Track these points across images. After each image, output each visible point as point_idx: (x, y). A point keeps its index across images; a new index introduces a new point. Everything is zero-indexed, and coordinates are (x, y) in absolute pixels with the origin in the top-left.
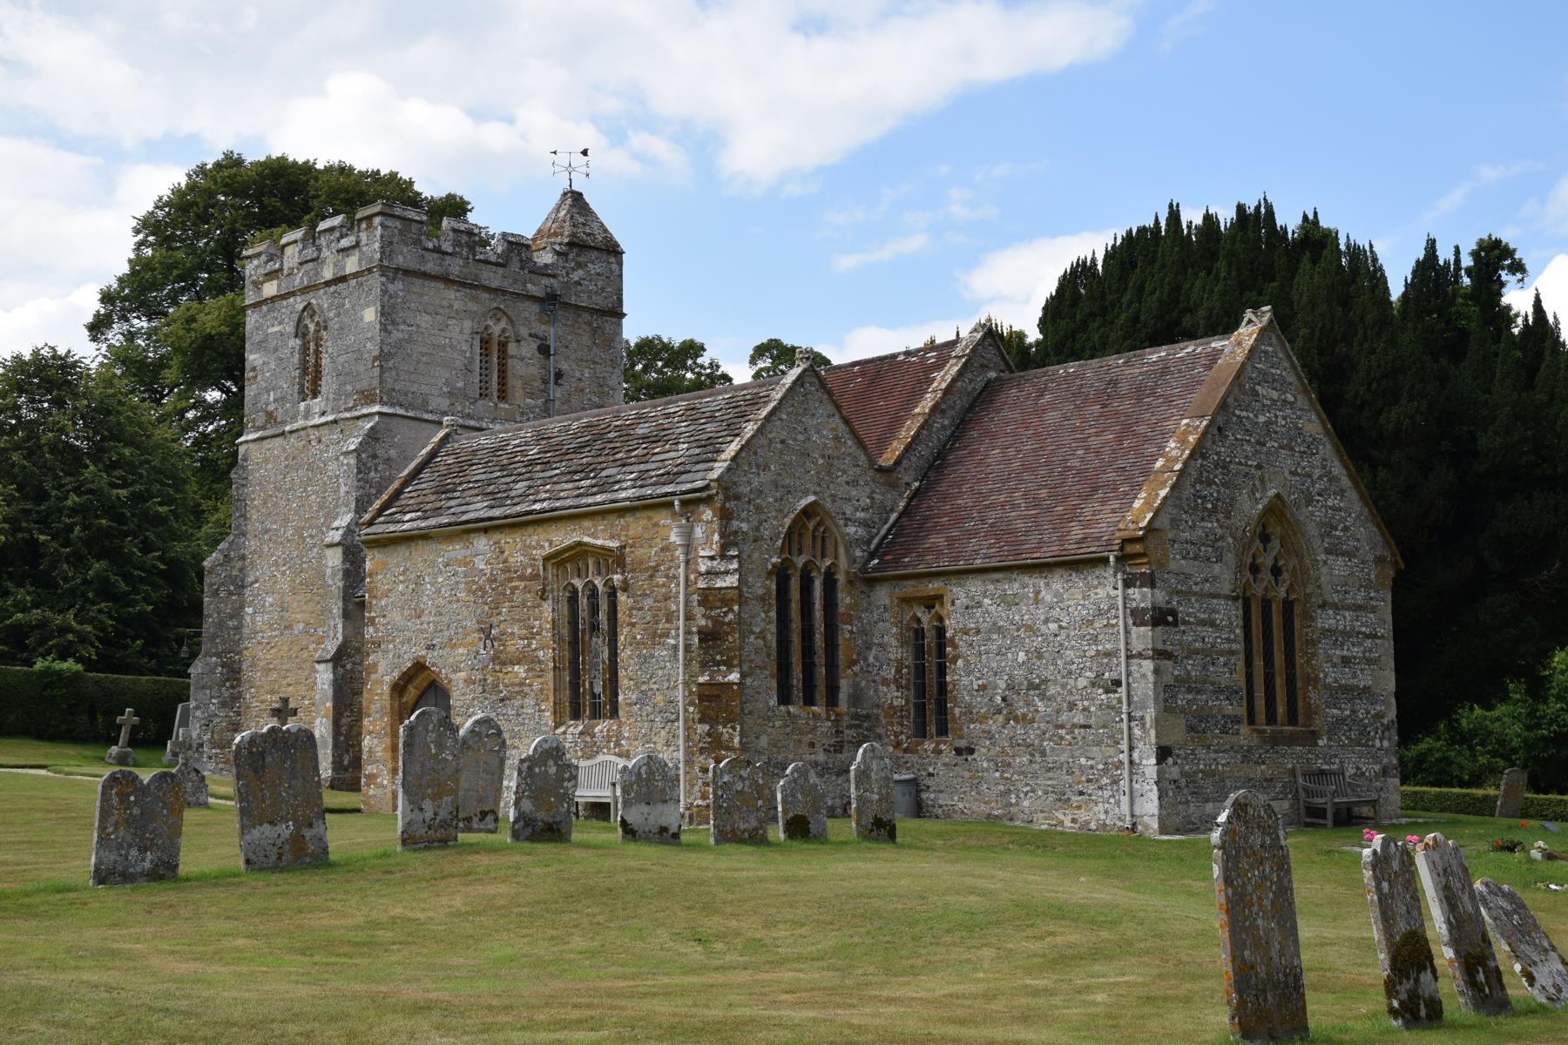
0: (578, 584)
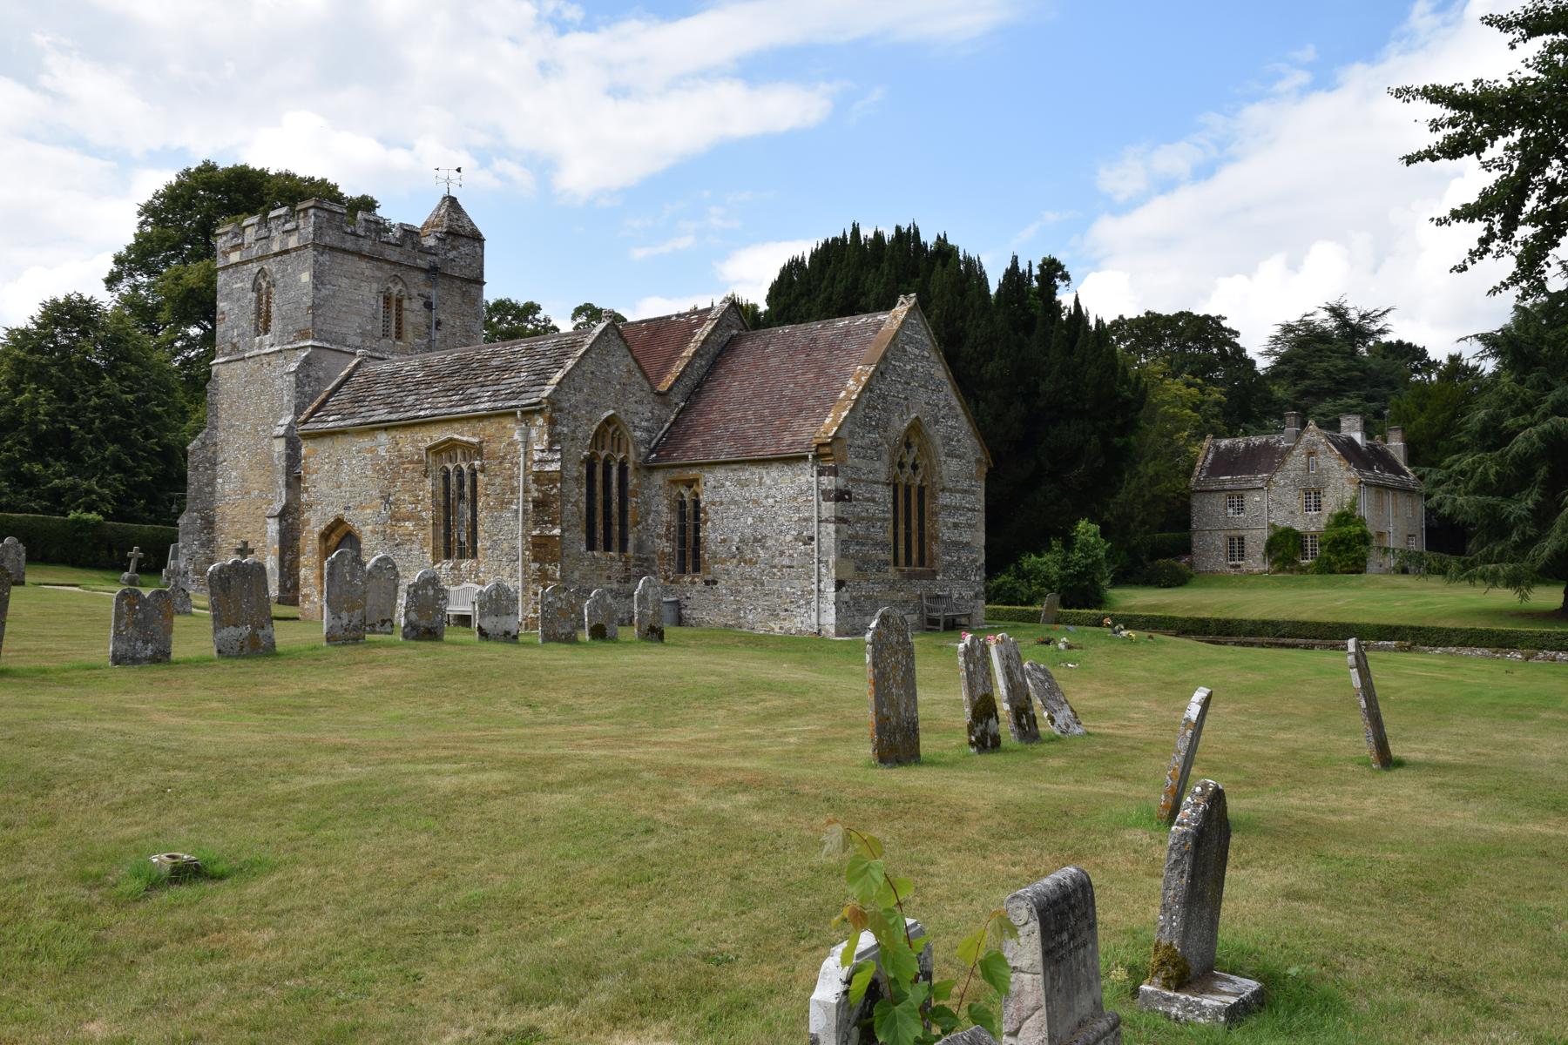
0: (450, 467)
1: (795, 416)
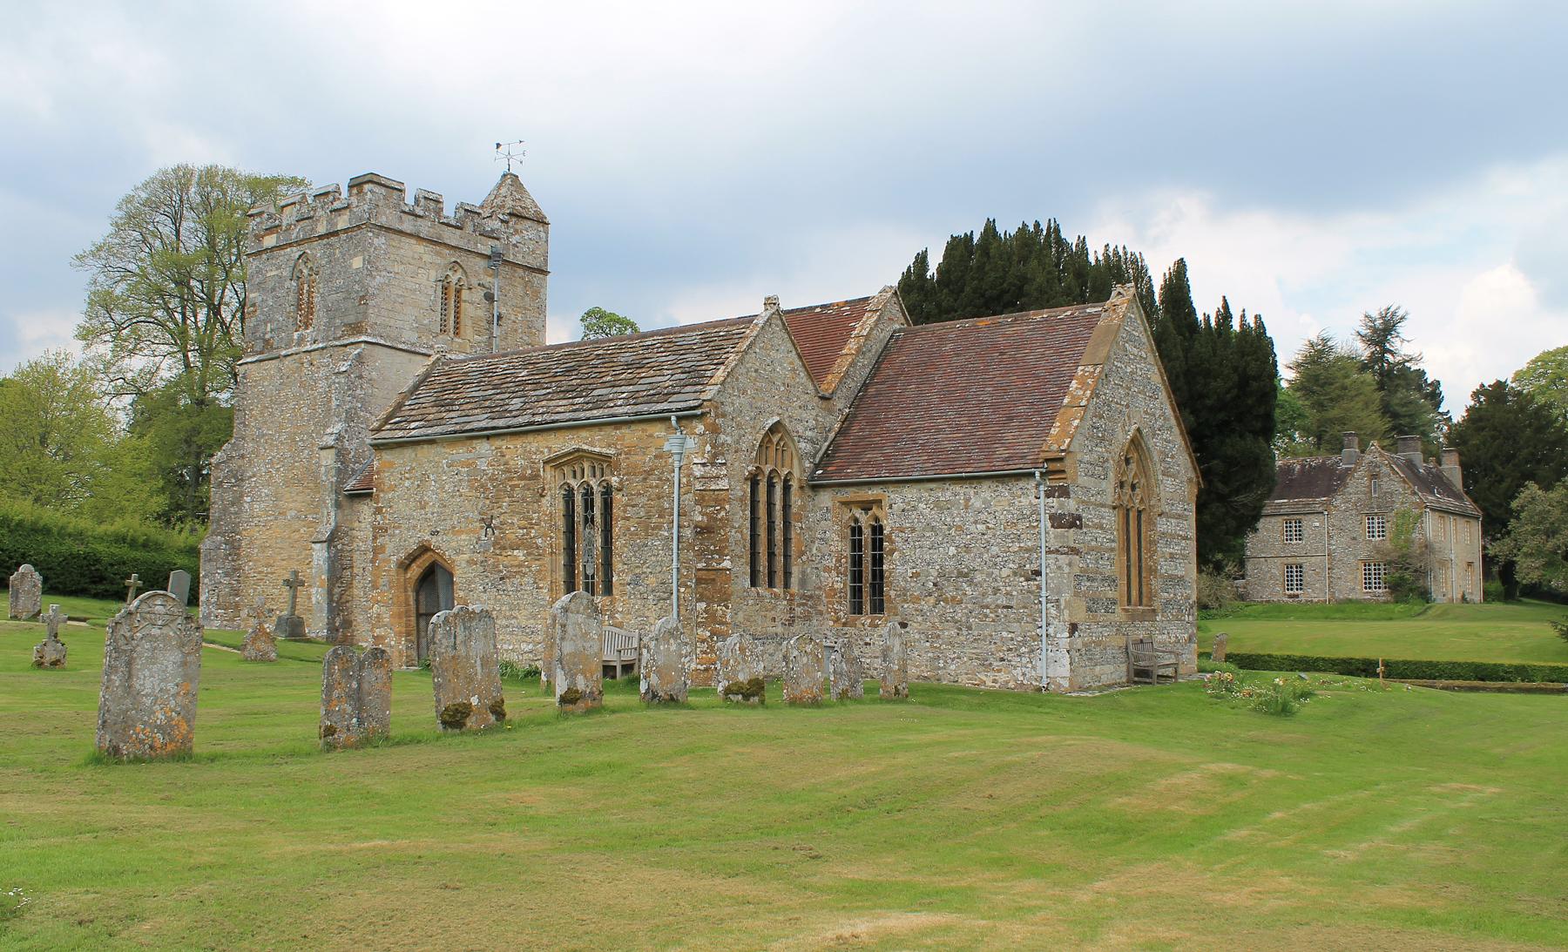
0: (574, 484)
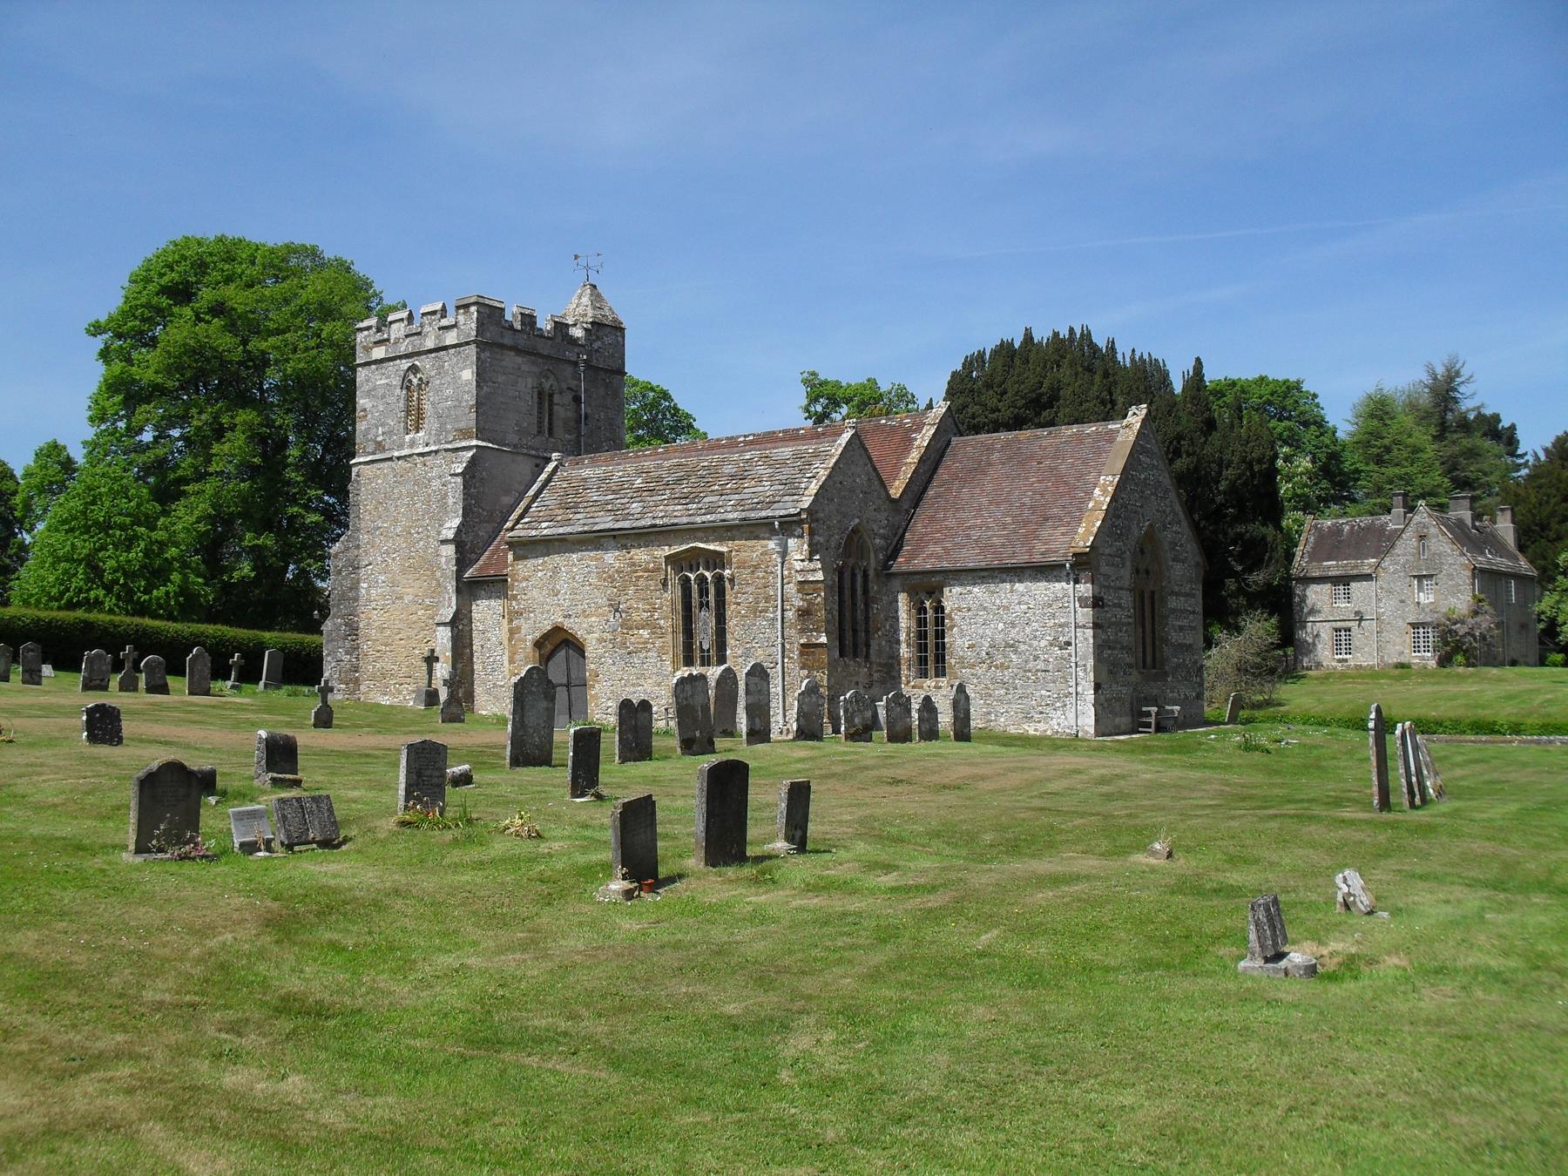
1: (1041, 524)
